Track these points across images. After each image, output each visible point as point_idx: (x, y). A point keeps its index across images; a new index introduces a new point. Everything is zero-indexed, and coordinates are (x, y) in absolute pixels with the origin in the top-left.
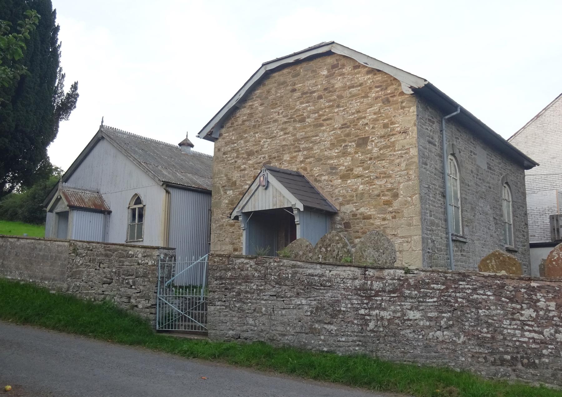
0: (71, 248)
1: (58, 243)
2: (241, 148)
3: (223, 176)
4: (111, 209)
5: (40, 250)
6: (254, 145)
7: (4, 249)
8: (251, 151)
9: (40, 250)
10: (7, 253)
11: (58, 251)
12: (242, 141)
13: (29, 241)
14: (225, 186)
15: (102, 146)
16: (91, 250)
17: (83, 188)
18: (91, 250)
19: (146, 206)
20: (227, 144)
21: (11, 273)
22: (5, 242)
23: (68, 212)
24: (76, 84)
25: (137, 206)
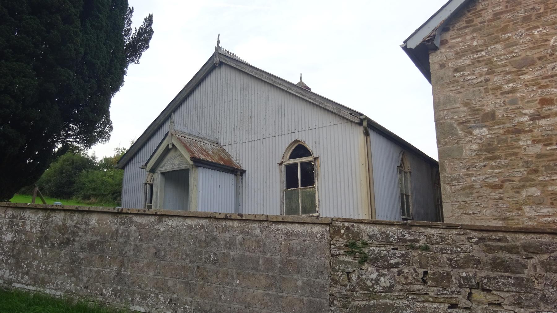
0: (341, 242)
1: (289, 227)
2: (498, 56)
3: (458, 105)
4: (243, 168)
5: (230, 245)
6: (531, 48)
7: (121, 240)
8: (526, 58)
9: (230, 245)
10: (129, 250)
11: (291, 250)
12: (499, 46)
13: (189, 222)
14: (468, 121)
15: (222, 74)
16: (426, 249)
17: (200, 135)
18: (426, 249)
19: (321, 160)
20: (459, 55)
21: (144, 297)
22: (122, 224)
23: (188, 169)
24: (151, 17)
25: (298, 161)
